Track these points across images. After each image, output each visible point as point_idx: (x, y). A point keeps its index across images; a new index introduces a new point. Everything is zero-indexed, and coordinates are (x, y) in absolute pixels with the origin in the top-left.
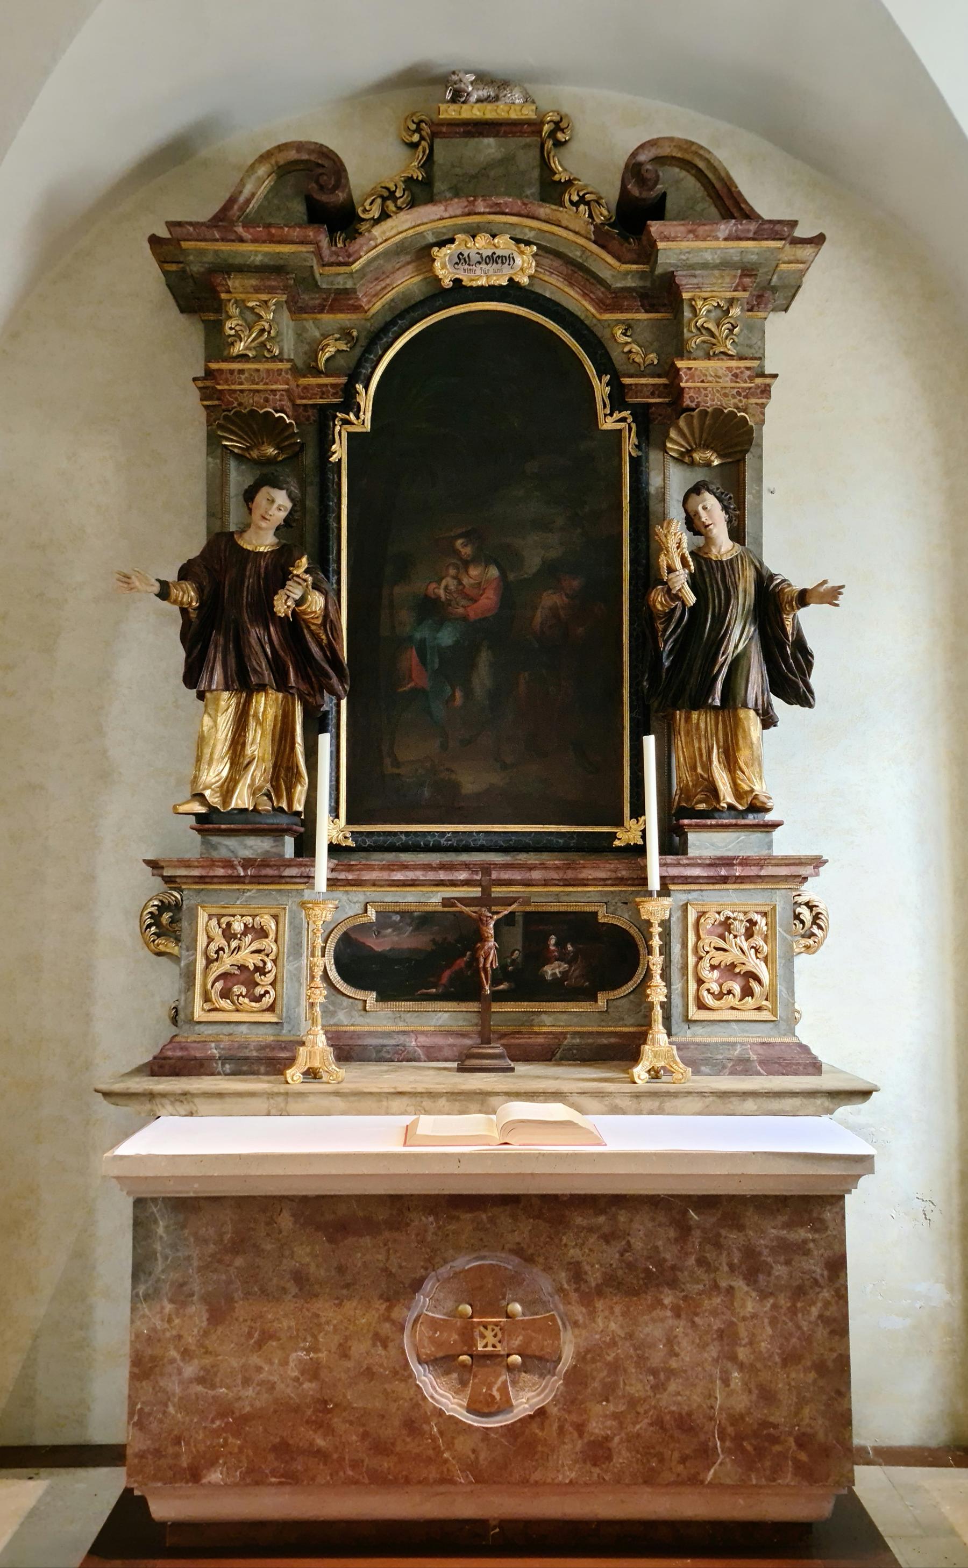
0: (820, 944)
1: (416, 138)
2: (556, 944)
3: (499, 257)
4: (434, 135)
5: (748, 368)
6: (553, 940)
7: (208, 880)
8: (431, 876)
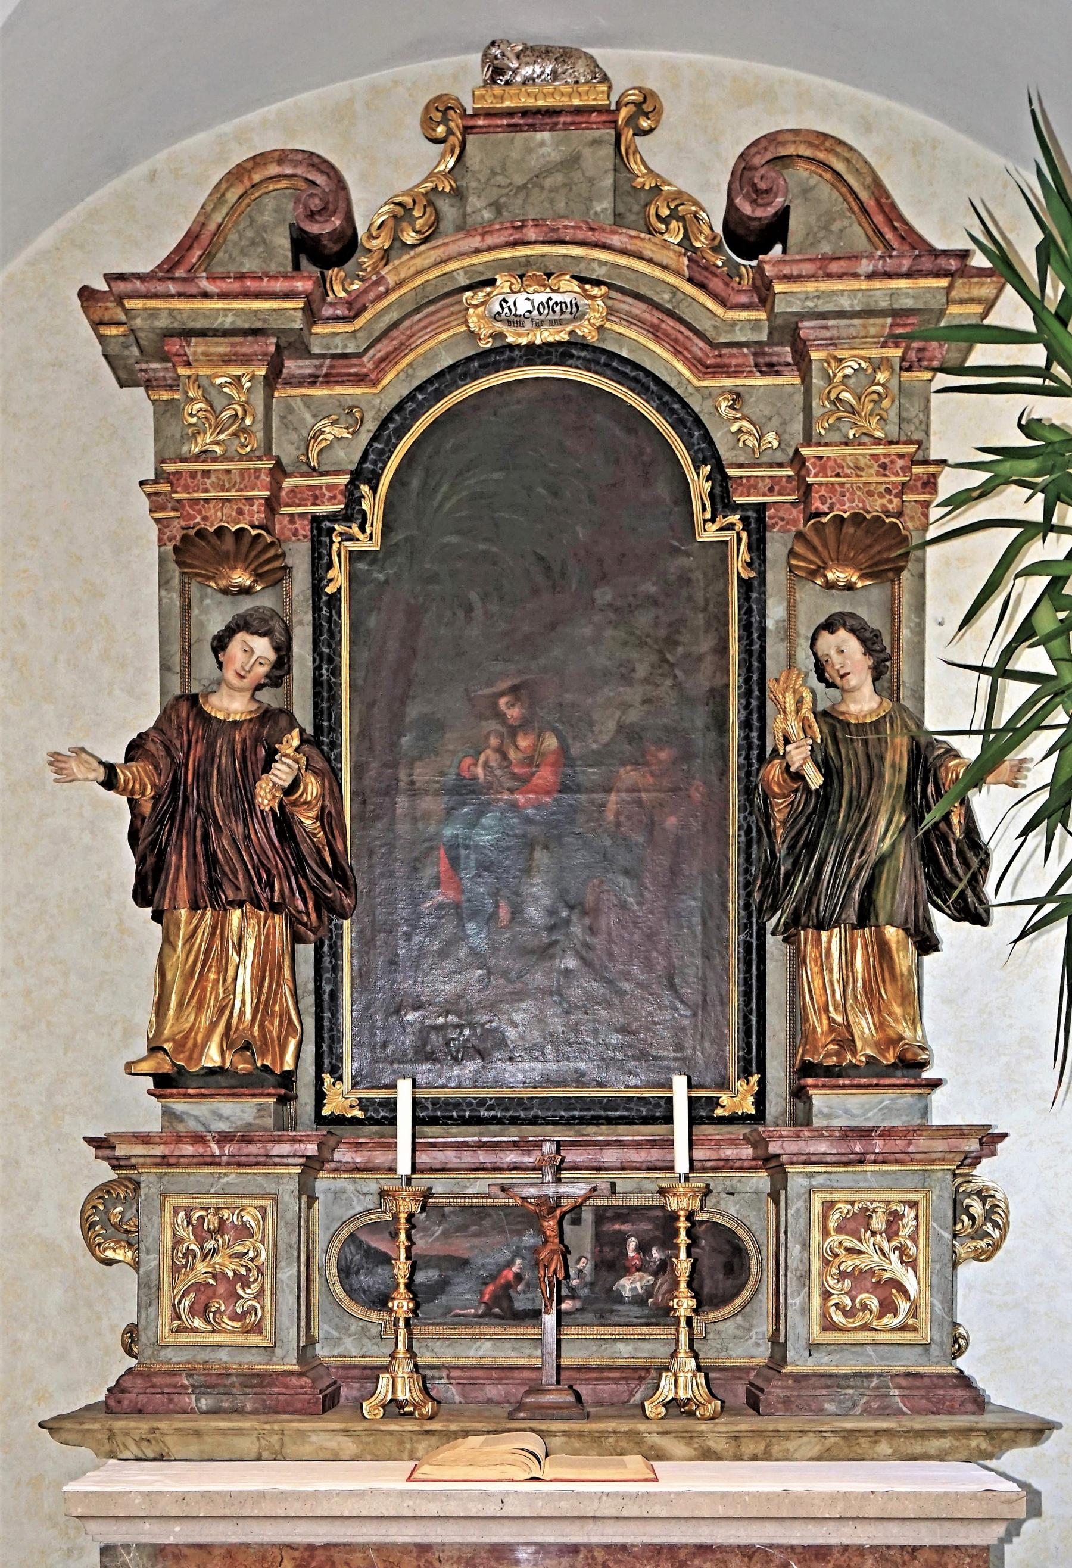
0: (996, 1246)
1: (441, 130)
2: (637, 1250)
3: (556, 303)
4: (467, 130)
5: (901, 456)
6: (632, 1243)
7: (172, 1161)
8: (468, 1158)
